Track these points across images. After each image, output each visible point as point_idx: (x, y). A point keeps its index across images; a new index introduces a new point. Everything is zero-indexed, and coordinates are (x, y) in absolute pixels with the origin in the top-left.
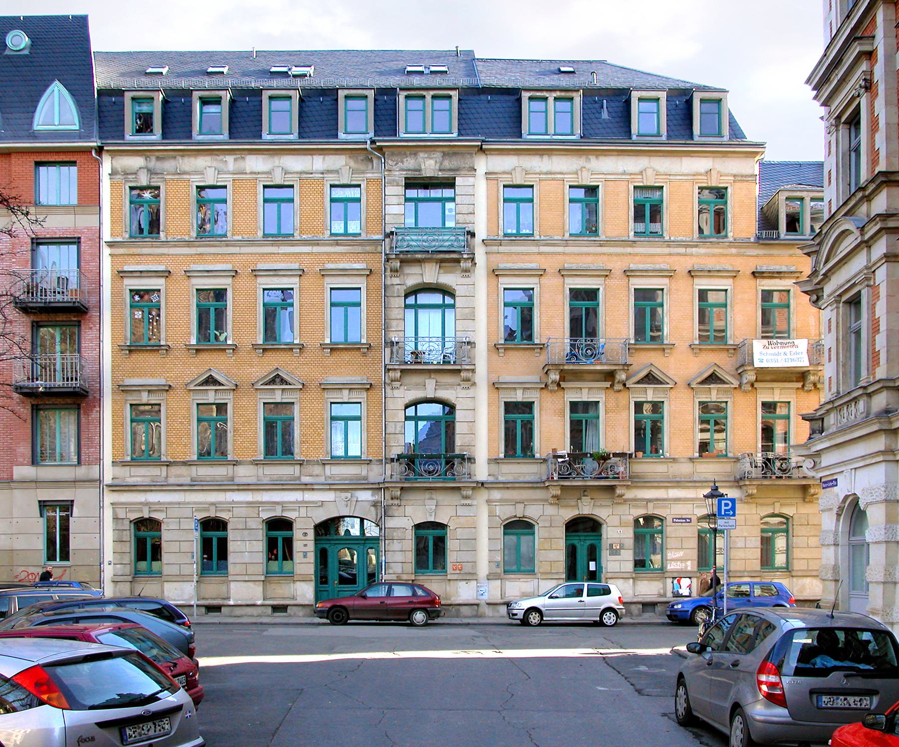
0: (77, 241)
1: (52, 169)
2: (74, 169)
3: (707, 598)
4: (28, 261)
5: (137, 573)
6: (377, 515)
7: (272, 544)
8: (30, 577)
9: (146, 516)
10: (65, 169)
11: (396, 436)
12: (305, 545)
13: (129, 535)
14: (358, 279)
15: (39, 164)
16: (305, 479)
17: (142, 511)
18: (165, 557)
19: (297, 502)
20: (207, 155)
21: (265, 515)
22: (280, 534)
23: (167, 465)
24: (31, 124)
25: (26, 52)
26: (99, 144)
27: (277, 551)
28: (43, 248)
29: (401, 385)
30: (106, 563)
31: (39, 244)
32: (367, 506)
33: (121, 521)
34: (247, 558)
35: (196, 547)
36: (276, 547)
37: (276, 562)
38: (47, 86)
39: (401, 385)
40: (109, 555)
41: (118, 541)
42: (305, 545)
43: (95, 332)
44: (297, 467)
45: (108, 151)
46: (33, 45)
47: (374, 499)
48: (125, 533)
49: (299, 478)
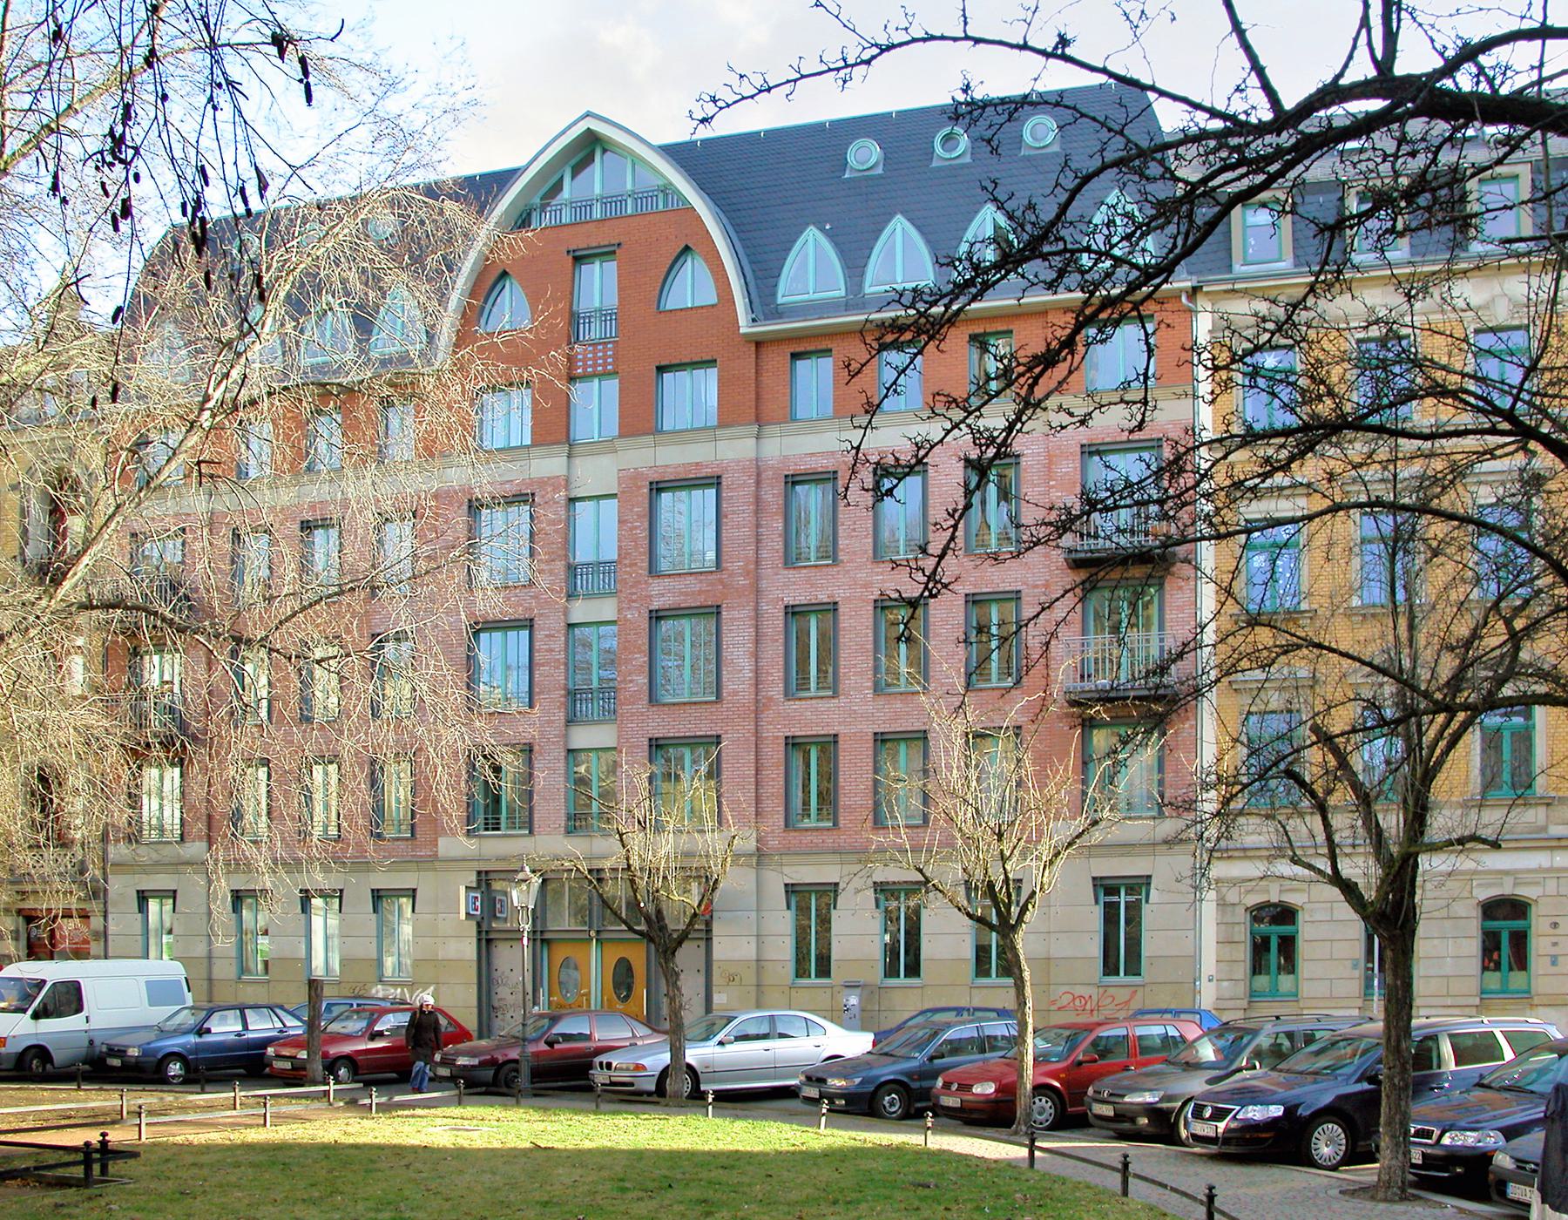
0: (716, 482)
1: (684, 376)
2: (713, 373)
4: (1075, 483)
5: (1253, 994)
7: (1490, 944)
8: (1077, 1002)
9: (1274, 899)
10: (699, 373)
12: (1555, 944)
13: (1242, 934)
15: (795, 356)
16: (1555, 830)
17: (1268, 892)
18: (1304, 967)
19: (1540, 870)
20: (1375, 286)
21: (1484, 894)
22: (1505, 926)
23: (1548, 805)
24: (774, 295)
25: (879, 171)
26: (1195, 284)
27: (1499, 956)
28: (666, 497)
31: (794, 483)
33: (1230, 909)
34: (1448, 967)
35: (1473, 947)
36: (1498, 948)
37: (1497, 974)
38: (805, 229)
40: (1209, 965)
41: (1225, 942)
42: (1555, 944)
43: (1187, 595)
44: (1542, 810)
45: (1208, 293)
46: (887, 159)
48: (1237, 928)
49: (1545, 829)
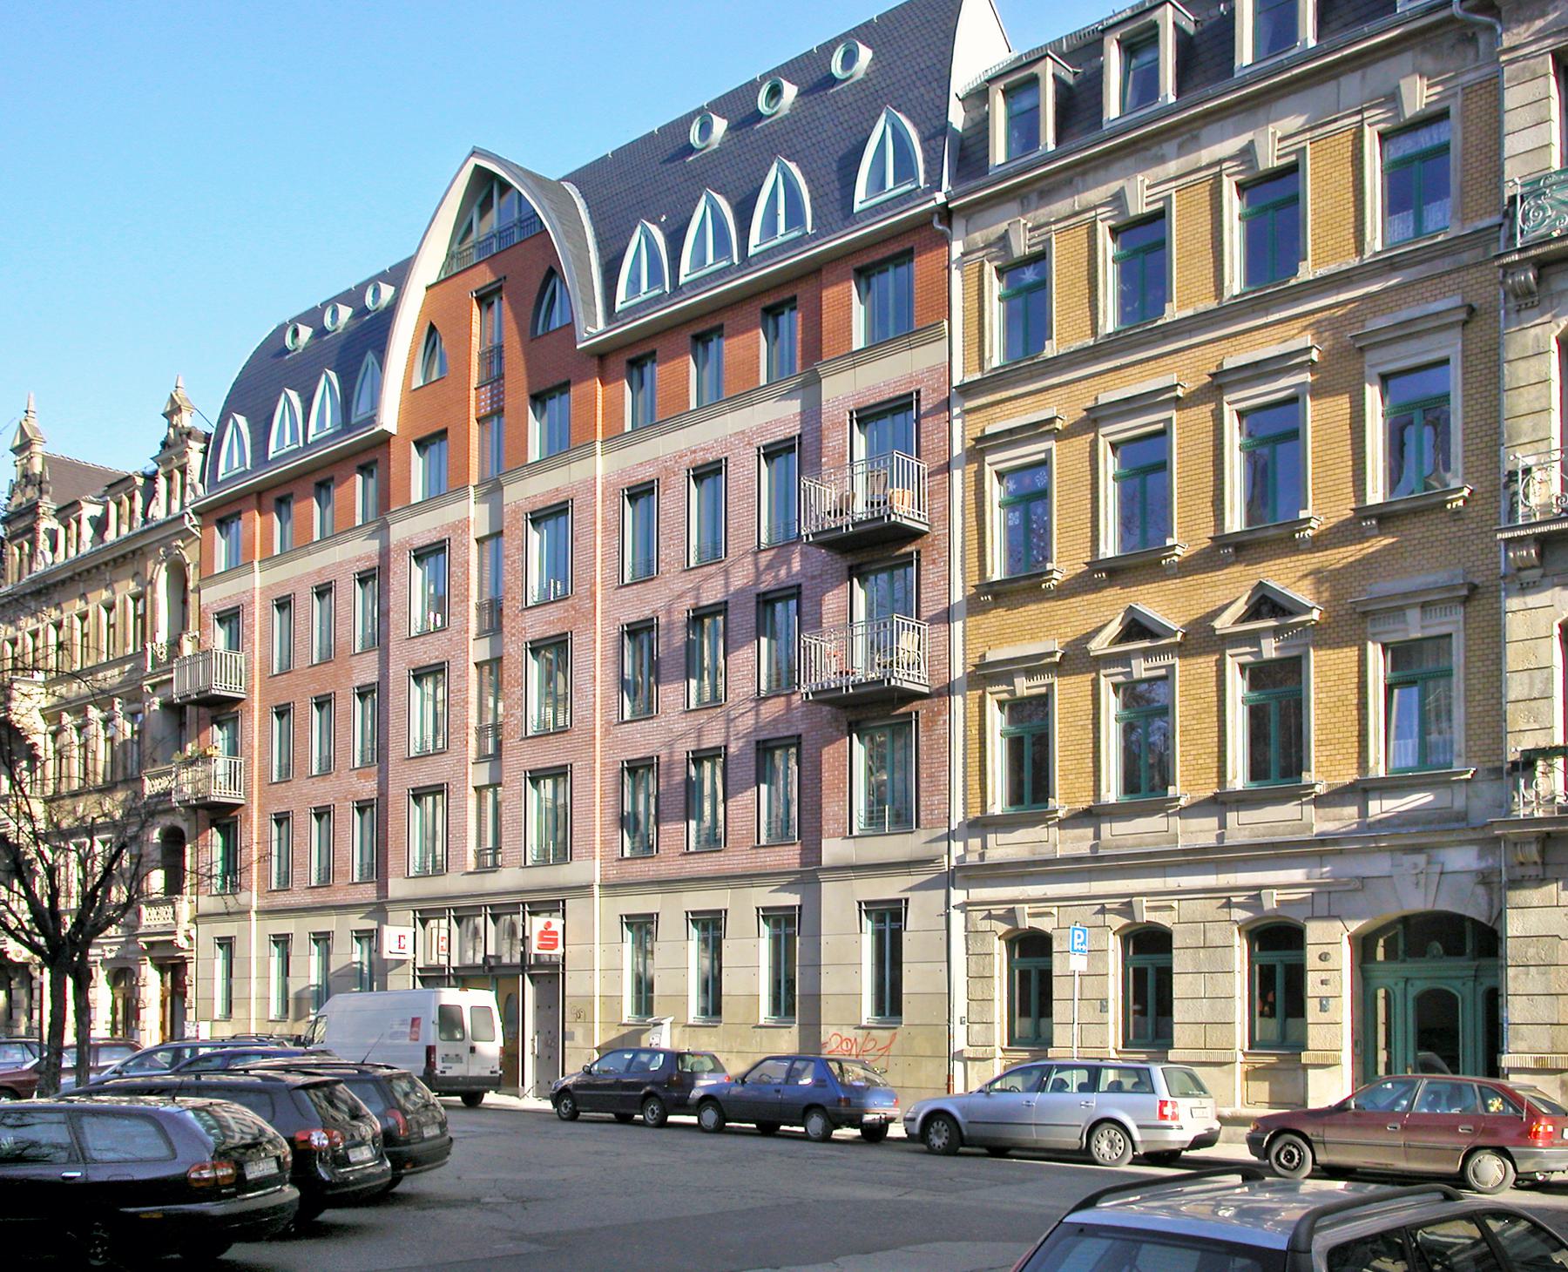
3: (328, 1117)
6: (1491, 905)
11: (1533, 704)
14: (1442, 337)
29: (1544, 576)
30: (957, 1021)
31: (1543, 267)
32: (1468, 882)
39: (1544, 576)
47: (1483, 865)
